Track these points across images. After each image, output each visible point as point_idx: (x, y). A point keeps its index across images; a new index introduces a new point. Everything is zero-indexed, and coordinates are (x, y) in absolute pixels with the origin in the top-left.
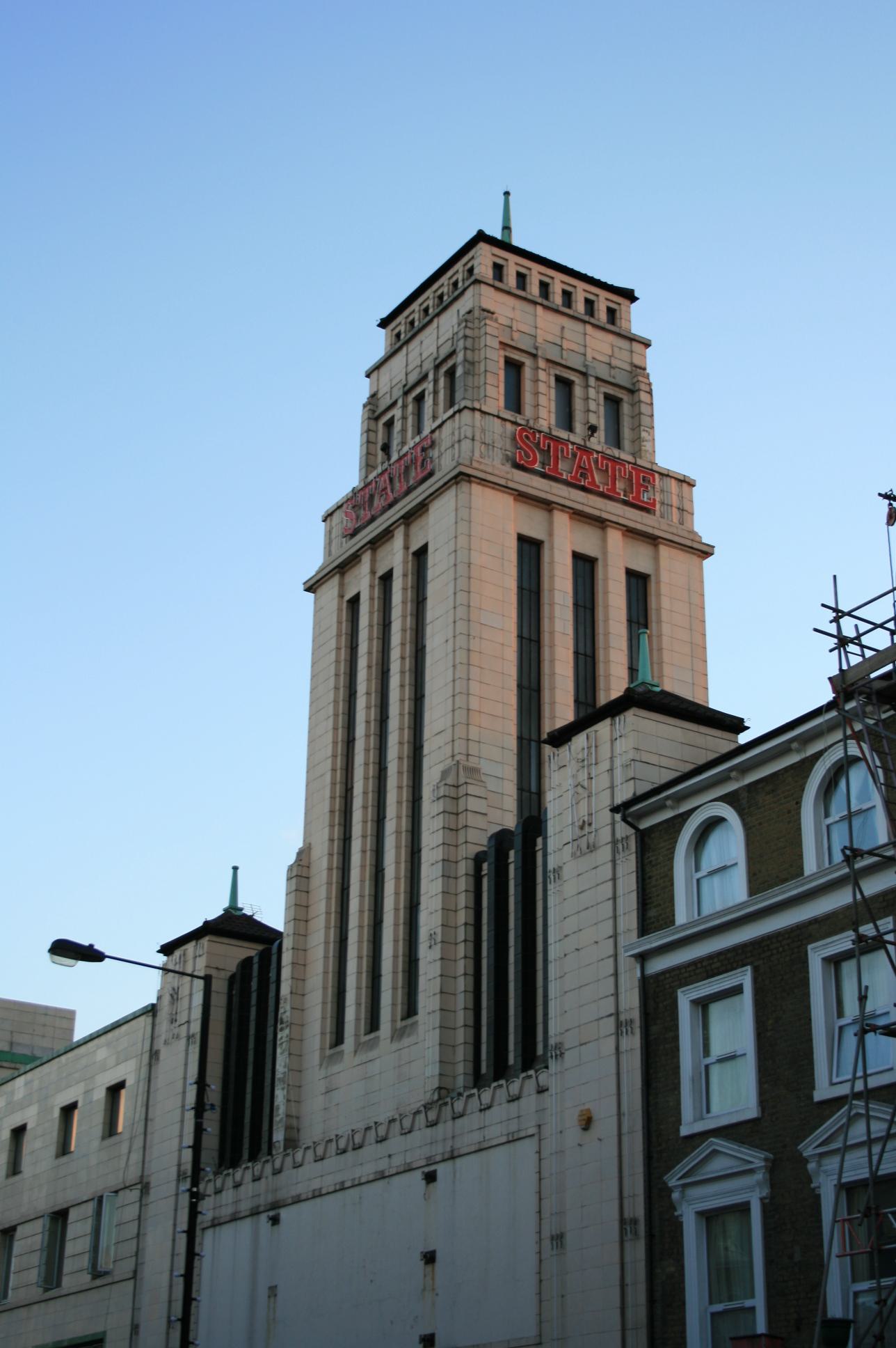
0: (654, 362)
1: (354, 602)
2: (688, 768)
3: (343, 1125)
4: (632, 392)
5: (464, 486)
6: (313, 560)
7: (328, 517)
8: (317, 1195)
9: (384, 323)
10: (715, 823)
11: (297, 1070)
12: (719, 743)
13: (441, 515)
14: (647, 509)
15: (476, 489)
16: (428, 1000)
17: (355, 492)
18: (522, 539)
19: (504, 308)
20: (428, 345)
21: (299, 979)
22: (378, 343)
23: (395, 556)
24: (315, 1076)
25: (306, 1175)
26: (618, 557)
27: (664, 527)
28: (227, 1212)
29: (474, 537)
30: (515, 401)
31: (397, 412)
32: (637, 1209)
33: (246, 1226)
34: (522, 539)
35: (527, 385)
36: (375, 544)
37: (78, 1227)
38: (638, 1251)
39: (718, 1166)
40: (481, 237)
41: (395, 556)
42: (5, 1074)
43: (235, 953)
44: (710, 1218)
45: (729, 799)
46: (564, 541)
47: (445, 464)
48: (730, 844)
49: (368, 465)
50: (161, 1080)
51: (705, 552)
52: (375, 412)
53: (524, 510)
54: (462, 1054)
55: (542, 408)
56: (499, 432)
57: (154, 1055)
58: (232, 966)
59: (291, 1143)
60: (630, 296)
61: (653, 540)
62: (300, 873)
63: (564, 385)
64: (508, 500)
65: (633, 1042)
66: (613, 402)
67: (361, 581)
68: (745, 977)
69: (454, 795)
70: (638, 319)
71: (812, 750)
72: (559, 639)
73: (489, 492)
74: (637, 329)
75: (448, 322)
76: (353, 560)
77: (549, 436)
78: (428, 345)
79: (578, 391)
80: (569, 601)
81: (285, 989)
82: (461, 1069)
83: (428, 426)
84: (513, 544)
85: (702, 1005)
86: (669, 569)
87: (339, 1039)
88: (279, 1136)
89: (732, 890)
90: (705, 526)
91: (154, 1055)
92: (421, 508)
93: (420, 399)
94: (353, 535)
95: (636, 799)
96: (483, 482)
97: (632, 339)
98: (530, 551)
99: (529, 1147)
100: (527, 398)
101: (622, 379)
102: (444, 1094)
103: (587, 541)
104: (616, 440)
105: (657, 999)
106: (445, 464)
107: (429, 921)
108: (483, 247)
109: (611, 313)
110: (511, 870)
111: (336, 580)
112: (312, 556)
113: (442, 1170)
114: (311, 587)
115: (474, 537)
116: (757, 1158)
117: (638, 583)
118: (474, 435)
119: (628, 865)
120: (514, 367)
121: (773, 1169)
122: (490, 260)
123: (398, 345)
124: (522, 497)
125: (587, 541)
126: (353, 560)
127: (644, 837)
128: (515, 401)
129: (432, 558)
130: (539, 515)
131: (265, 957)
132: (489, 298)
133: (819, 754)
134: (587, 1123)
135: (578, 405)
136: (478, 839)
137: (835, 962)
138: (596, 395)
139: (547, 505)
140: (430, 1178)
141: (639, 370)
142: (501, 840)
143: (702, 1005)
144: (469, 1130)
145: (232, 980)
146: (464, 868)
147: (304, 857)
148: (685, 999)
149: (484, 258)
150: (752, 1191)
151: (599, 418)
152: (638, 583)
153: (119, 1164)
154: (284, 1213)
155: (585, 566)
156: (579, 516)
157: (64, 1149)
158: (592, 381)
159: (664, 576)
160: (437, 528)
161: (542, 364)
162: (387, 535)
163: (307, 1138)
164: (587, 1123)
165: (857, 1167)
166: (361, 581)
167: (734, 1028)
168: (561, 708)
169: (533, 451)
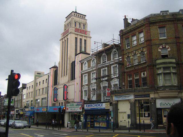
0: (88, 22)
1: (63, 42)
6: (60, 38)
8: (60, 88)
9: (66, 18)
10: (86, 63)
11: (59, 79)
12: (89, 56)
13: (69, 35)
16: (68, 74)
19: (75, 18)
20: (69, 20)
21: (59, 72)
22: (65, 20)
23: (66, 39)
24: (60, 79)
26: (83, 38)
29: (71, 38)
31: (69, 24)
35: (77, 24)
36: (64, 37)
38: (80, 93)
39: (85, 87)
40: (73, 12)
41: (66, 39)
43: (56, 69)
44: (85, 91)
45: (87, 61)
47: (69, 32)
48: (87, 65)
52: (65, 26)
53: (76, 35)
54: (70, 78)
55: (78, 27)
56: (74, 29)
58: (55, 70)
59: (59, 84)
60: (86, 16)
61: (87, 37)
62: (59, 64)
63: (80, 24)
64: (74, 34)
65: (80, 78)
66: (84, 25)
67: (64, 40)
68: (87, 74)
69: (70, 58)
70: (86, 18)
75: (70, 19)
77: (78, 29)
78: (69, 20)
79: (81, 24)
80: (79, 42)
81: (58, 72)
82: (70, 79)
83: (69, 28)
85: (85, 76)
86: (88, 39)
87: (67, 75)
88: (58, 83)
89: (87, 68)
90: (91, 36)
93: (68, 25)
97: (86, 20)
98: (76, 38)
99: (74, 85)
100: (77, 25)
103: (81, 37)
105: (82, 75)
106: (69, 32)
107: (68, 68)
110: (73, 64)
111: (62, 40)
115: (71, 38)
116: (87, 87)
117: (85, 40)
118: (72, 29)
119: (80, 65)
121: (88, 88)
122: (13, 70)
124: (75, 34)
125: (81, 37)
126: (63, 38)
129: (68, 39)
130: (77, 35)
131: (57, 70)
132: (73, 17)
135: (81, 26)
136: (71, 62)
137: (85, 76)
138: (82, 25)
139: (78, 35)
142: (73, 62)
143: (113, 67)
144: (70, 84)
145: (71, 63)
146: (70, 64)
147: (60, 62)
148: (84, 75)
149: (73, 13)
150: (107, 85)
151: (83, 27)
152: (85, 40)
155: (81, 39)
156: (80, 35)
157: (43, 83)
159: (87, 40)
160: (69, 37)
162: (65, 37)
163: (60, 84)
165: (104, 85)
166: (64, 40)
167: (87, 78)
168: (78, 52)
169: (77, 30)
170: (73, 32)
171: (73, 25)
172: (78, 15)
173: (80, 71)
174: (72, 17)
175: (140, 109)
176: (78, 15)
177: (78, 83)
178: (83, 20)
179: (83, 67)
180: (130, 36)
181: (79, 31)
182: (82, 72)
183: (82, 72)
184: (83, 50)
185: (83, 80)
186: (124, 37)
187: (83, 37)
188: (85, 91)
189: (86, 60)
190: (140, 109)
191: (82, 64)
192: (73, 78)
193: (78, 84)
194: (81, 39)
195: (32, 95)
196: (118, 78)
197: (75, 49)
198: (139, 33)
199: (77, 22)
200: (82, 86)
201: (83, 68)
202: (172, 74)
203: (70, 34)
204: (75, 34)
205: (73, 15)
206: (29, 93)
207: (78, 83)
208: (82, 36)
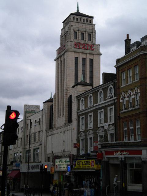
0: (96, 28)
1: (59, 63)
2: (85, 91)
3: (59, 126)
4: (92, 33)
5: (68, 52)
7: (57, 51)
14: (93, 50)
15: (69, 52)
17: (59, 48)
18: (75, 57)
21: (55, 109)
25: (55, 132)
26: (88, 57)
27: (95, 52)
28: (49, 134)
29: (70, 58)
30: (76, 38)
32: (77, 139)
33: (51, 136)
34: (75, 57)
37: (37, 135)
41: (62, 59)
42: (143, 43)
45: (84, 98)
46: (81, 57)
49: (61, 46)
50: (43, 119)
51: (101, 54)
55: (79, 39)
57: (43, 115)
59: (54, 127)
60: (93, 18)
61: (93, 54)
63: (83, 34)
65: (77, 121)
66: (90, 35)
68: (113, 107)
70: (94, 21)
71: (109, 85)
72: (80, 70)
73: (71, 52)
74: (94, 23)
76: (61, 57)
79: (85, 34)
82: (67, 121)
84: (74, 58)
86: (95, 58)
87: (58, 117)
88: (53, 127)
89: (84, 108)
91: (43, 115)
92: (63, 54)
94: (59, 54)
95: (78, 96)
96: (70, 51)
98: (77, 59)
101: (91, 31)
102: (65, 124)
103: (84, 56)
104: (90, 40)
105: (79, 116)
108: (72, 15)
109: (90, 21)
112: (55, 56)
113: (65, 132)
114: (55, 60)
115: (70, 58)
117: (91, 60)
118: (70, 45)
120: (76, 33)
121: (94, 133)
123: (64, 27)
125: (84, 56)
127: (78, 100)
128: (76, 38)
133: (109, 86)
134: (74, 129)
140: (64, 133)
141: (94, 29)
145: (69, 98)
146: (68, 99)
148: (80, 117)
152: (91, 60)
153: (38, 128)
154: (54, 135)
155: (84, 60)
156: (83, 53)
158: (86, 32)
159: (95, 59)
161: (79, 31)
163: (56, 127)
164: (74, 129)
170: (72, 48)
171: (73, 37)
172: (80, 19)
173: (77, 110)
174: (69, 24)
175: (123, 169)
176: (80, 19)
177: (75, 128)
178: (88, 26)
179: (98, 99)
180: (126, 69)
181: (81, 47)
182: (79, 112)
183: (79, 112)
184: (80, 79)
185: (108, 115)
186: (120, 69)
187: (88, 55)
188: (82, 140)
189: (83, 96)
190: (123, 169)
191: (79, 101)
192: (70, 121)
193: (75, 130)
194: (84, 60)
195: (21, 143)
196: (114, 125)
197: (75, 76)
198: (122, 72)
199: (77, 32)
200: (79, 132)
201: (80, 108)
202: (35, 153)
203: (66, 53)
204: (75, 52)
205: (72, 19)
206: (39, 132)
207: (75, 128)
208: (86, 53)
